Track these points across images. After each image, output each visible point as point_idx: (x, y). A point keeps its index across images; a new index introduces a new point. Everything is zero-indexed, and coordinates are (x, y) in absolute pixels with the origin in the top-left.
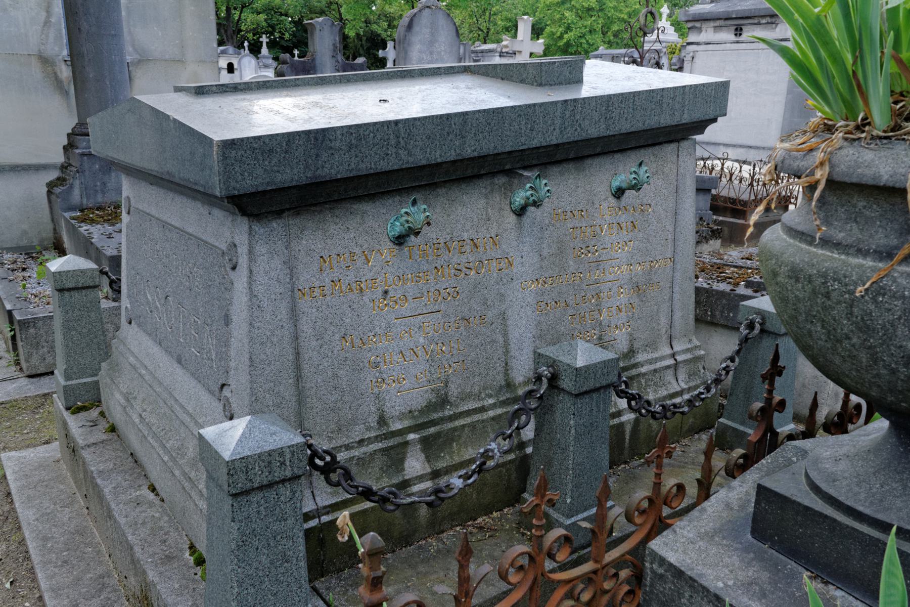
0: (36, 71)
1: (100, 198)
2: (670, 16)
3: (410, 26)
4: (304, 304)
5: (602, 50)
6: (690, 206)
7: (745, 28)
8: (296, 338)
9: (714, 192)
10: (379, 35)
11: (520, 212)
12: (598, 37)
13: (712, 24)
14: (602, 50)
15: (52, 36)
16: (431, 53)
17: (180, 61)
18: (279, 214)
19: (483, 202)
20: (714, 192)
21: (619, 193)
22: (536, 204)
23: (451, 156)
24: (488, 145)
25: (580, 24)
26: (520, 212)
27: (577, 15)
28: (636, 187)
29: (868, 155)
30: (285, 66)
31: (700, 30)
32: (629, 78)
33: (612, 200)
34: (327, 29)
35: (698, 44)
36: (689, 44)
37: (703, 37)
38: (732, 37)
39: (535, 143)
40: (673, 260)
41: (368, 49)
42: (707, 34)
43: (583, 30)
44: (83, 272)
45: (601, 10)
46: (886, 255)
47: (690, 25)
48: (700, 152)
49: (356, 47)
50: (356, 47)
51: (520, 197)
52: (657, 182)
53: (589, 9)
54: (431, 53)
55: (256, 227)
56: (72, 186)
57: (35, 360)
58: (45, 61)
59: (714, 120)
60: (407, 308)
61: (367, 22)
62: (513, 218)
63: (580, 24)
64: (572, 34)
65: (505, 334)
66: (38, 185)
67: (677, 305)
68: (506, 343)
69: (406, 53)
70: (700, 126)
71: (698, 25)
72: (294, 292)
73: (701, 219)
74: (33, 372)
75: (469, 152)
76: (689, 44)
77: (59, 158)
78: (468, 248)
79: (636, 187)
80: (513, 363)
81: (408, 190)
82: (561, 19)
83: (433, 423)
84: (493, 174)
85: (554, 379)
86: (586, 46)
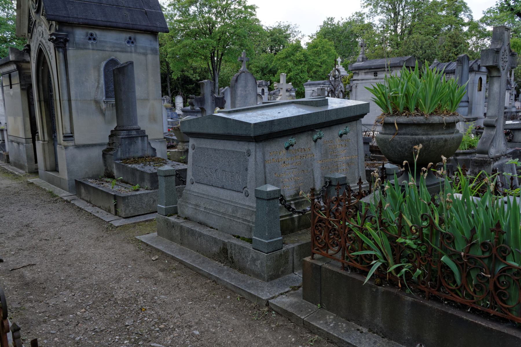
0: (93, 106)
1: (127, 156)
2: (342, 62)
3: (236, 80)
4: (267, 165)
5: (309, 81)
6: (362, 149)
7: (378, 73)
8: (265, 173)
9: (370, 144)
10: (188, 77)
11: (315, 141)
12: (306, 75)
13: (364, 71)
14: (309, 81)
15: (99, 92)
16: (246, 91)
17: (147, 99)
18: (261, 141)
19: (306, 138)
20: (370, 144)
21: (341, 136)
22: (320, 138)
23: (300, 126)
24: (341, 116)
25: (296, 68)
26: (315, 141)
27: (294, 64)
28: (346, 133)
29: (389, 118)
30: (193, 100)
31: (358, 74)
32: (341, 103)
33: (339, 138)
34: (209, 85)
35: (358, 80)
36: (354, 80)
37: (360, 77)
38: (373, 77)
39: (319, 122)
40: (358, 155)
41: (182, 84)
42: (362, 76)
43: (298, 71)
44: (171, 170)
45: (306, 61)
46: (394, 134)
47: (354, 72)
48: (364, 128)
49: (176, 84)
50: (176, 84)
51: (315, 137)
52: (351, 132)
53: (300, 61)
54: (246, 91)
55: (257, 145)
56: (118, 151)
57: (127, 212)
58: (97, 102)
59: (366, 114)
60: (289, 166)
61: (183, 71)
62: (313, 143)
63: (296, 68)
64: (292, 73)
65: (313, 176)
66: (97, 152)
67: (360, 170)
68: (314, 178)
69: (235, 91)
70: (362, 116)
71: (357, 72)
72: (264, 161)
73: (366, 155)
74: (126, 216)
75: (304, 125)
76: (354, 80)
77: (107, 141)
78: (303, 151)
79: (346, 133)
80: (316, 184)
81: (290, 135)
82: (286, 66)
83: (297, 199)
84: (308, 131)
85: (330, 182)
86: (299, 79)
